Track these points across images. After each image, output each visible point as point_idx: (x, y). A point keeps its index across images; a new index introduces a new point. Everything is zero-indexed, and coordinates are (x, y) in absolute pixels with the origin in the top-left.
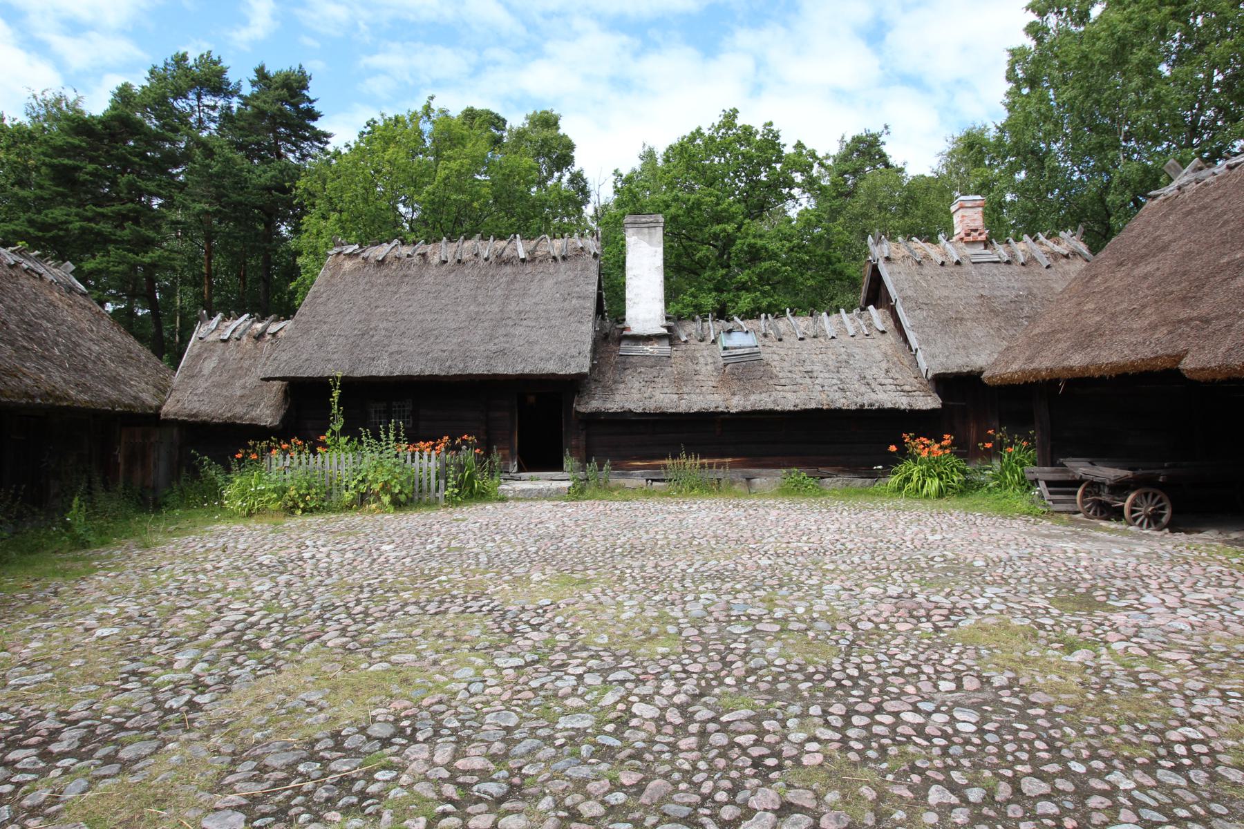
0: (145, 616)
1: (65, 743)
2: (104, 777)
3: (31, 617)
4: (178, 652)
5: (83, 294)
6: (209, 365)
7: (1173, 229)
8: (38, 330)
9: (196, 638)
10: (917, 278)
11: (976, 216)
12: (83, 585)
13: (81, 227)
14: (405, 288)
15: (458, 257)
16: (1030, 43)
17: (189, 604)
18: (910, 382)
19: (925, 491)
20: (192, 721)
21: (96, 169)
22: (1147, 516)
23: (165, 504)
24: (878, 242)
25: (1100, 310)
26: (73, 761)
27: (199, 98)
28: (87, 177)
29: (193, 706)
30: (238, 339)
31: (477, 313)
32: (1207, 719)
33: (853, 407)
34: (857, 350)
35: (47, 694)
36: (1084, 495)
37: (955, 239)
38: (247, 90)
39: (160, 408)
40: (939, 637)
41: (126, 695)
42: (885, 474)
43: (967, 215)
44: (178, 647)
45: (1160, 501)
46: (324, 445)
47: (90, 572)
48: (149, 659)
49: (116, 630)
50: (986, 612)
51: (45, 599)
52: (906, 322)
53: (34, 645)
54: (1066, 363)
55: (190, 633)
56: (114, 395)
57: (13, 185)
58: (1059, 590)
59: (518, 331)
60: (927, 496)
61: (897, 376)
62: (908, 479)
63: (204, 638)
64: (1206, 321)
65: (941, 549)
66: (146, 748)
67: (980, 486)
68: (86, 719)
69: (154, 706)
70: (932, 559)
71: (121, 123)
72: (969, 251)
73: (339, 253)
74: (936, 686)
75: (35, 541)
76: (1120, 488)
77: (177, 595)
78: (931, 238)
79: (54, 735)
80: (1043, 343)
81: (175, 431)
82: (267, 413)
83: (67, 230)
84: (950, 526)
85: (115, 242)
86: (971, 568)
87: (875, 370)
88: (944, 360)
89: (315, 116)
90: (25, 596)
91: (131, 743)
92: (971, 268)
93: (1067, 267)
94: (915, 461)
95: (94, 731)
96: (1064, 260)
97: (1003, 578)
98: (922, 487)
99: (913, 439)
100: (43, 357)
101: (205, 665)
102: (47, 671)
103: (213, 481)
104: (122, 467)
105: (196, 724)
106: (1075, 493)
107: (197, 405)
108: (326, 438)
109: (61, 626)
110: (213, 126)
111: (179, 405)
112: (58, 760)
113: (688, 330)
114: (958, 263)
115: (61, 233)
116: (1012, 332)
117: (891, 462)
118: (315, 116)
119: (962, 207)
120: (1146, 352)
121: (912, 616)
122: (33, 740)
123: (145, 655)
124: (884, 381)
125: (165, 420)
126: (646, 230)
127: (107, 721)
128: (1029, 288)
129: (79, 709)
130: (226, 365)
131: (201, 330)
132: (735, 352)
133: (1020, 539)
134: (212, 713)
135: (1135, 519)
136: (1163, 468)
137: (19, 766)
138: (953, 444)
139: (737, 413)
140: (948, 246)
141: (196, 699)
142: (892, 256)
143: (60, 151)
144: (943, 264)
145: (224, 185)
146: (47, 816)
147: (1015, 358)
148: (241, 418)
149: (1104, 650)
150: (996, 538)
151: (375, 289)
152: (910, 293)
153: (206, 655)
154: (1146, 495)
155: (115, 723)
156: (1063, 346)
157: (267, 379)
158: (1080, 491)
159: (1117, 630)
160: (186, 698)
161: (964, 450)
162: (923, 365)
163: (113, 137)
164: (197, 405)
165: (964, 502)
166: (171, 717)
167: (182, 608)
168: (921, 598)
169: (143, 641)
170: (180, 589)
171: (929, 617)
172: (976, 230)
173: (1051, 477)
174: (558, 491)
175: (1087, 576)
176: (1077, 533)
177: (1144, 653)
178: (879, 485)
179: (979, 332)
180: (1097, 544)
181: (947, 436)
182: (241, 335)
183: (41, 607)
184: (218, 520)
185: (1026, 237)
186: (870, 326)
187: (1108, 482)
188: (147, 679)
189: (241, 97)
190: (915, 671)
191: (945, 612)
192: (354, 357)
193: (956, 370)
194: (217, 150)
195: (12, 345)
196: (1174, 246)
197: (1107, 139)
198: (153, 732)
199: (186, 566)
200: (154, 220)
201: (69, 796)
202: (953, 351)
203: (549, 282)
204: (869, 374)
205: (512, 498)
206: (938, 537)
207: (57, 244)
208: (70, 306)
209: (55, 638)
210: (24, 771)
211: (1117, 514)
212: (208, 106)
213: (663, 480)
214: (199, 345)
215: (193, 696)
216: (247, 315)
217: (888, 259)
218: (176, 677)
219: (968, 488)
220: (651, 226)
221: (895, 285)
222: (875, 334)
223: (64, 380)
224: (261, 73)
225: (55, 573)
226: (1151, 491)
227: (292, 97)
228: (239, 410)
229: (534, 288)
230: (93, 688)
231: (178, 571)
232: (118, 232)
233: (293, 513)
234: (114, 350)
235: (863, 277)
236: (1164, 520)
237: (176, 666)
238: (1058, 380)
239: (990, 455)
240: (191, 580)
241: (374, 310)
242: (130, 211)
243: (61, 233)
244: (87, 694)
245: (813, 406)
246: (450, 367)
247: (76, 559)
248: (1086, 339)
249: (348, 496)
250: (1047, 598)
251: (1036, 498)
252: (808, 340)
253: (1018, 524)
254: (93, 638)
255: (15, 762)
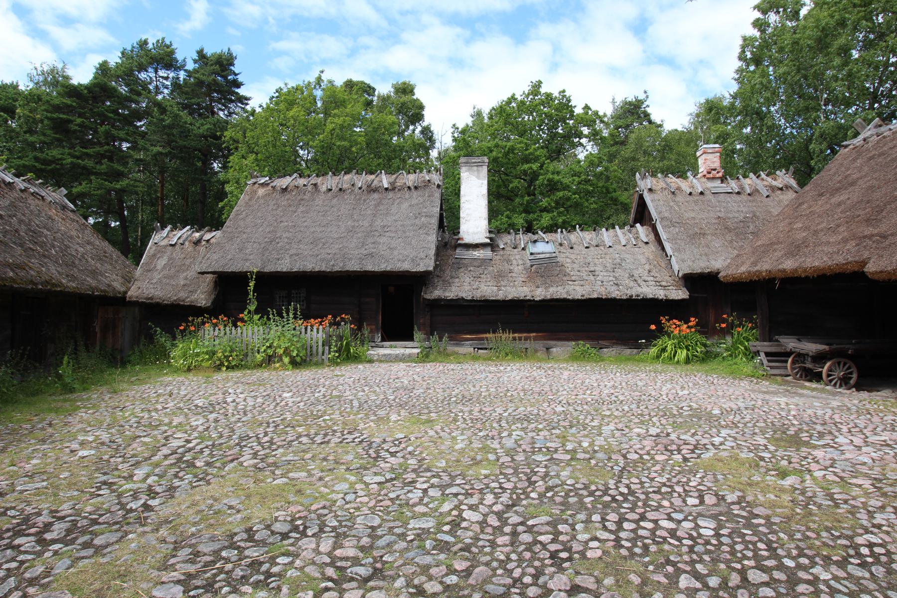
0: (114, 442)
1: (56, 533)
2: (83, 558)
3: (33, 441)
4: (136, 468)
5: (73, 211)
6: (161, 263)
7: (860, 169)
8: (40, 236)
9: (150, 458)
10: (672, 204)
11: (715, 159)
12: (70, 419)
13: (72, 162)
14: (301, 209)
15: (340, 186)
16: (756, 33)
17: (145, 434)
18: (666, 279)
19: (676, 359)
20: (146, 518)
21: (83, 122)
22: (840, 379)
23: (129, 362)
24: (643, 177)
25: (806, 228)
26: (61, 546)
27: (156, 72)
28: (77, 128)
29: (147, 507)
30: (182, 244)
31: (353, 227)
32: (884, 528)
33: (624, 297)
34: (628, 256)
35: (43, 497)
36: (793, 362)
37: (699, 175)
38: (190, 66)
39: (126, 293)
40: (687, 466)
41: (99, 499)
42: (647, 346)
43: (708, 158)
44: (137, 464)
45: (849, 368)
46: (242, 320)
47: (75, 410)
48: (116, 473)
49: (93, 452)
50: (721, 447)
51: (43, 429)
52: (663, 236)
53: (34, 462)
54: (780, 267)
55: (146, 455)
56: (94, 283)
57: (25, 132)
58: (775, 432)
59: (383, 240)
60: (678, 362)
61: (657, 275)
62: (664, 350)
63: (155, 459)
64: (884, 237)
65: (688, 401)
66: (113, 538)
67: (717, 355)
68: (70, 516)
69: (119, 507)
70: (682, 408)
71: (100, 88)
72: (710, 184)
73: (255, 183)
74: (684, 501)
75: (36, 387)
76: (820, 358)
77: (137, 427)
78: (682, 175)
79: (47, 527)
80: (763, 252)
81: (137, 310)
82: (202, 297)
83: (62, 165)
84: (694, 385)
85: (96, 174)
86: (710, 415)
87: (640, 270)
88: (691, 264)
89: (238, 85)
90: (29, 426)
91: (102, 534)
92: (711, 197)
93: (781, 197)
94: (669, 336)
95: (76, 525)
96: (779, 192)
97: (733, 423)
98: (674, 356)
99: (668, 321)
100: (44, 256)
101: (156, 478)
102: (43, 481)
103: (164, 347)
104: (98, 335)
105: (149, 521)
106: (786, 362)
107: (153, 291)
108: (244, 315)
109: (53, 449)
110: (166, 91)
111: (140, 291)
112: (50, 545)
113: (505, 240)
114: (702, 193)
115: (58, 167)
116: (741, 244)
117: (651, 338)
118: (238, 85)
119: (704, 153)
120: (840, 259)
121: (667, 450)
122: (33, 530)
123: (113, 470)
124: (647, 278)
125: (130, 302)
126: (475, 168)
127: (86, 518)
128: (753, 212)
129: (65, 509)
130: (173, 263)
131: (156, 238)
132: (539, 256)
133: (746, 395)
134: (160, 513)
135: (831, 381)
136: (851, 344)
137: (22, 549)
138: (697, 325)
139: (540, 301)
140: (695, 181)
141: (149, 502)
142: (654, 188)
143: (57, 108)
144: (690, 194)
145: (172, 133)
146: (42, 585)
147: (743, 263)
148: (183, 301)
149: (808, 477)
150: (728, 393)
151: (280, 209)
152: (666, 215)
153: (157, 471)
154: (839, 363)
155: (91, 519)
156: (778, 254)
157: (203, 273)
158: (790, 360)
159: (817, 462)
160: (142, 501)
161: (705, 329)
162: (676, 267)
163: (95, 99)
164: (153, 291)
165: (705, 367)
166: (131, 515)
167: (140, 437)
168: (673, 436)
169: (112, 460)
170: (139, 423)
171: (679, 451)
172: (715, 170)
173: (769, 350)
174: (410, 355)
175: (795, 422)
176: (788, 391)
177: (838, 480)
178: (643, 354)
179: (717, 243)
180: (802, 399)
181: (692, 319)
182: (184, 241)
183: (40, 434)
184: (167, 374)
185: (751, 175)
186: (637, 238)
187: (811, 354)
188: (115, 487)
189: (186, 71)
190: (669, 490)
191: (691, 447)
192: (264, 257)
193: (699, 271)
194: (169, 108)
195: (22, 247)
196: (860, 182)
197: (812, 103)
198: (118, 526)
199: (143, 406)
200: (123, 158)
201: (58, 571)
202: (698, 257)
203: (405, 205)
204: (636, 273)
205: (377, 361)
206: (686, 392)
207: (52, 174)
208: (63, 219)
209: (50, 457)
210: (26, 552)
211: (816, 377)
212: (162, 77)
213: (486, 349)
214: (154, 248)
215: (147, 500)
216: (188, 227)
217: (650, 190)
218: (135, 486)
219: (708, 357)
220: (479, 165)
221: (656, 209)
222: (640, 244)
223: (59, 272)
224: (201, 53)
225: (50, 410)
226: (843, 360)
227: (223, 71)
228: (182, 295)
229: (394, 209)
230: (76, 493)
231: (137, 410)
232: (98, 167)
233: (220, 369)
234: (94, 251)
235: (632, 203)
236: (852, 382)
237: (135, 478)
238: (774, 279)
239: (727, 331)
240: (146, 416)
241: (277, 224)
242: (106, 151)
243: (58, 167)
244: (71, 498)
245: (595, 296)
246: (333, 265)
247: (65, 401)
248: (795, 249)
249: (259, 357)
250: (766, 438)
251: (758, 365)
252: (592, 248)
253: (745, 384)
254: (77, 458)
255: (20, 546)
